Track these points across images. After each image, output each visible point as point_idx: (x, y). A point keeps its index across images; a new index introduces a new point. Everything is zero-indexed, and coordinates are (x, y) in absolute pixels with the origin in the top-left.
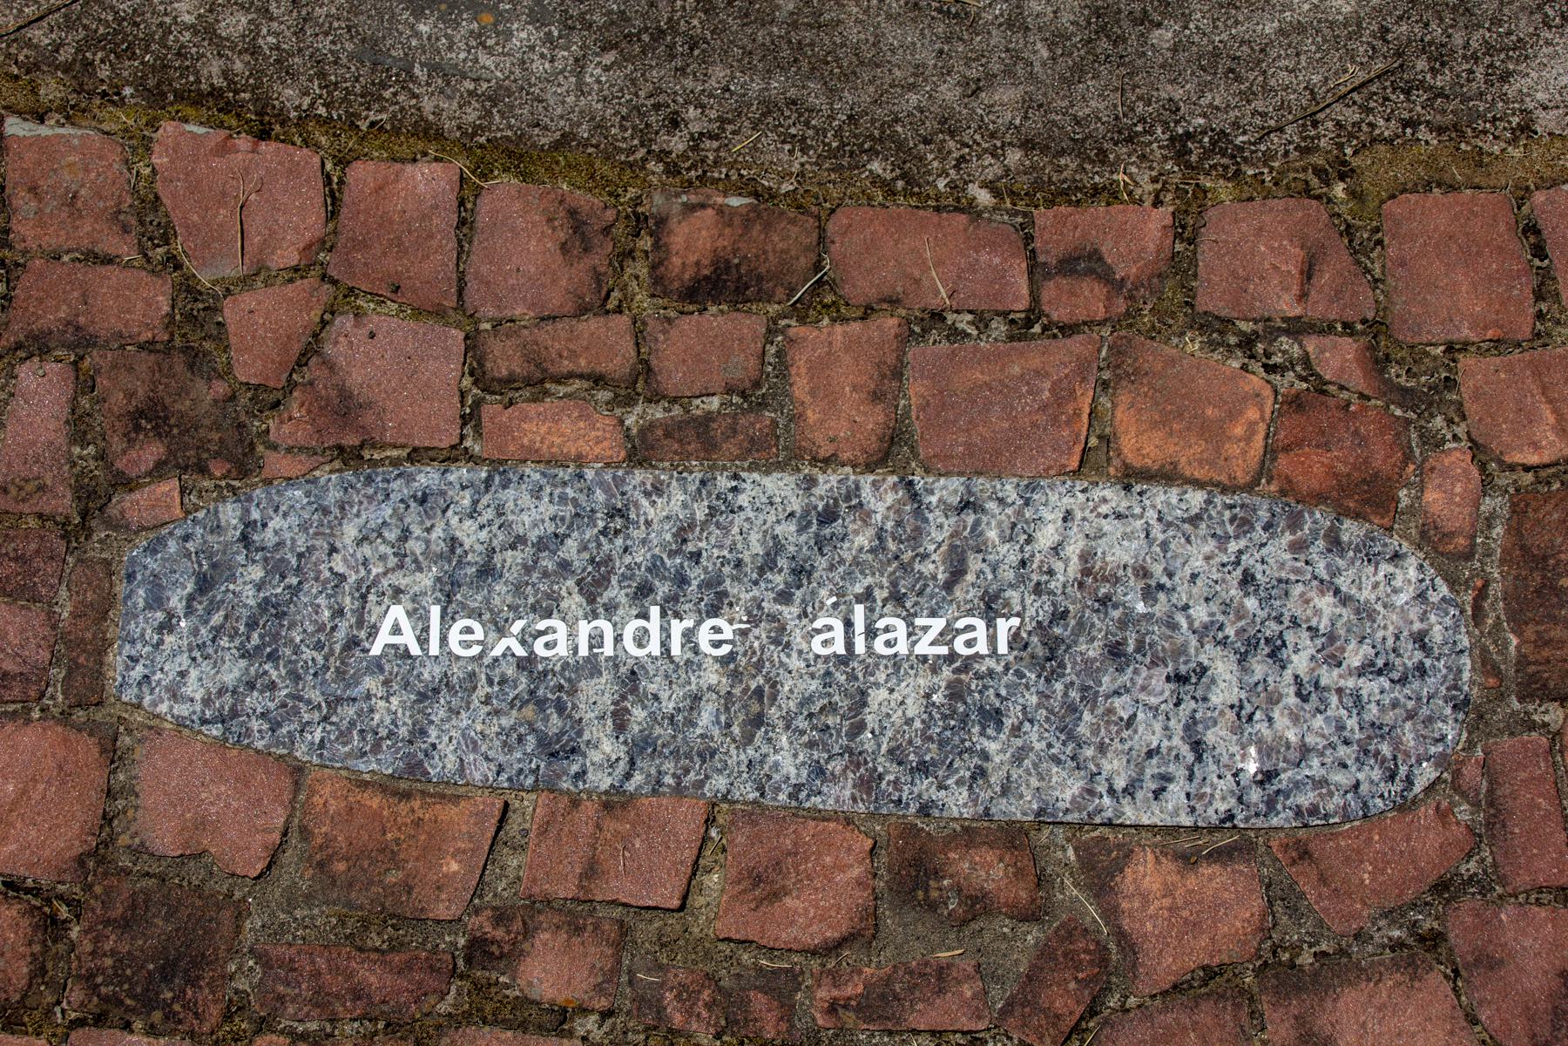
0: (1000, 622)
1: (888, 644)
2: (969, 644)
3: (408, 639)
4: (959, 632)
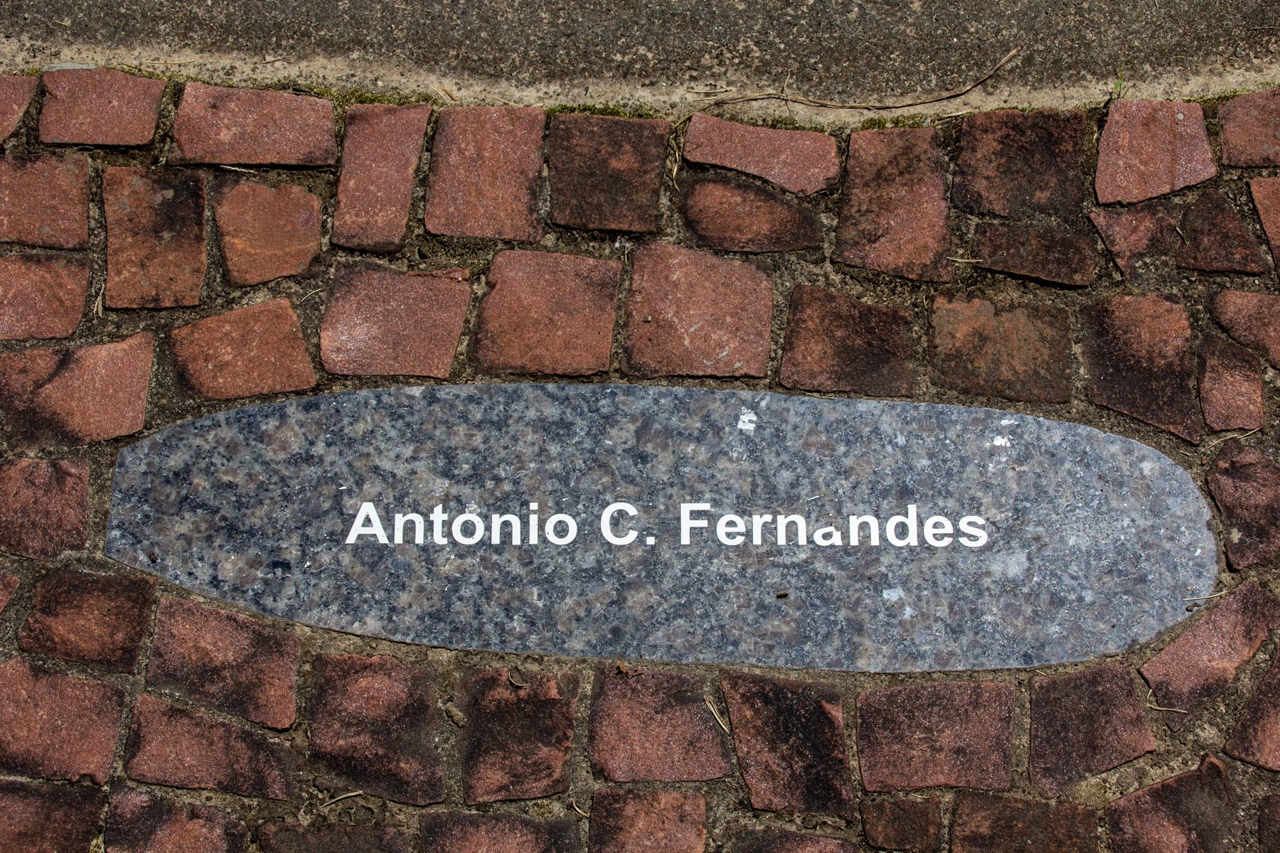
0: (852, 518)
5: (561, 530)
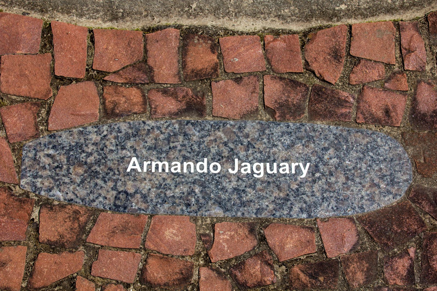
0: (145, 162)
1: (283, 170)
2: (176, 169)
3: (138, 167)
4: (242, 167)
5: (215, 167)
